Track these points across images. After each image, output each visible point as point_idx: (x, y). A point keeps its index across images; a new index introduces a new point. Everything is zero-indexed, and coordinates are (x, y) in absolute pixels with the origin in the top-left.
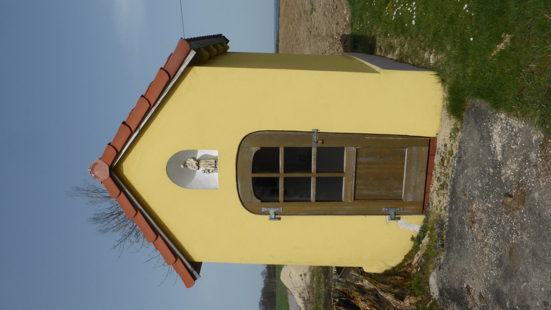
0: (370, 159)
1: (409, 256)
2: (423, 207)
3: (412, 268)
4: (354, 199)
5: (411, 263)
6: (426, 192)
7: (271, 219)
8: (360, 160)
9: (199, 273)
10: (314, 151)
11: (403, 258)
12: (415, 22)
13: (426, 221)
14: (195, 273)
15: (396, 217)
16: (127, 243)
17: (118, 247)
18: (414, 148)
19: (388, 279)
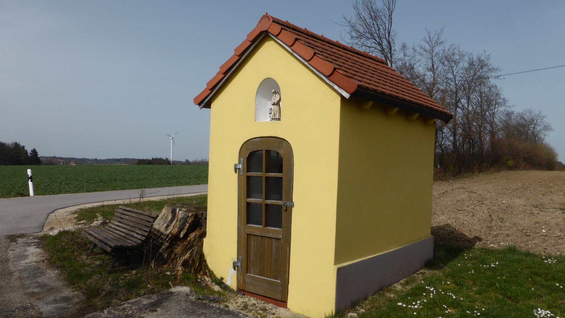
0: (274, 250)
1: (211, 275)
2: (242, 291)
3: (202, 275)
4: (248, 234)
5: (206, 275)
6: (252, 294)
7: (236, 165)
8: (274, 241)
9: (204, 107)
10: (280, 202)
11: (212, 269)
12: (400, 306)
13: (231, 290)
14: (203, 105)
15: (235, 266)
16: (348, 29)
17: (344, 21)
18: (280, 288)
19: (198, 256)
